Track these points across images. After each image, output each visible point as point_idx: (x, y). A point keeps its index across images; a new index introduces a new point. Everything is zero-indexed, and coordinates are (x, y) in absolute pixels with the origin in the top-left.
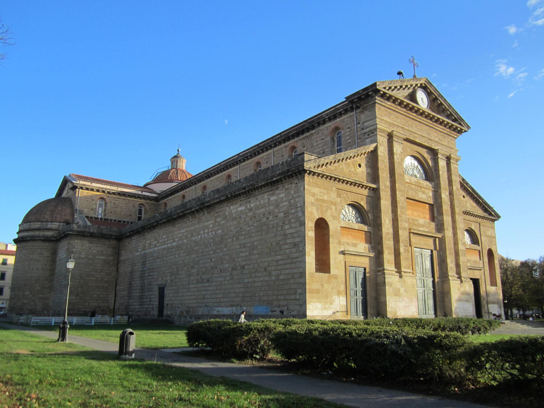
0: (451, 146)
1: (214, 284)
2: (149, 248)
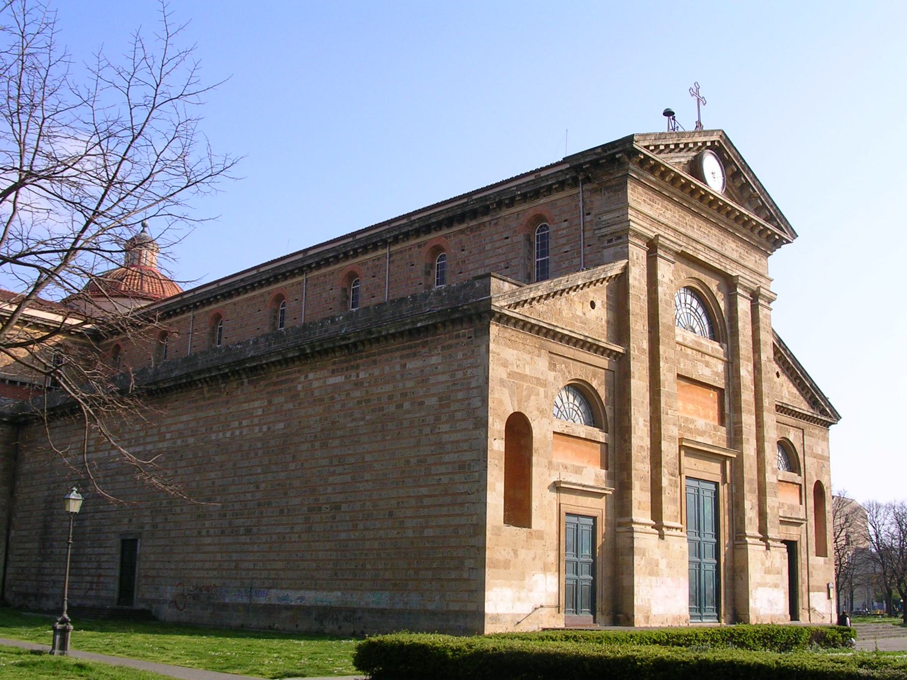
0: (761, 271)
1: (264, 538)
2: (97, 451)
